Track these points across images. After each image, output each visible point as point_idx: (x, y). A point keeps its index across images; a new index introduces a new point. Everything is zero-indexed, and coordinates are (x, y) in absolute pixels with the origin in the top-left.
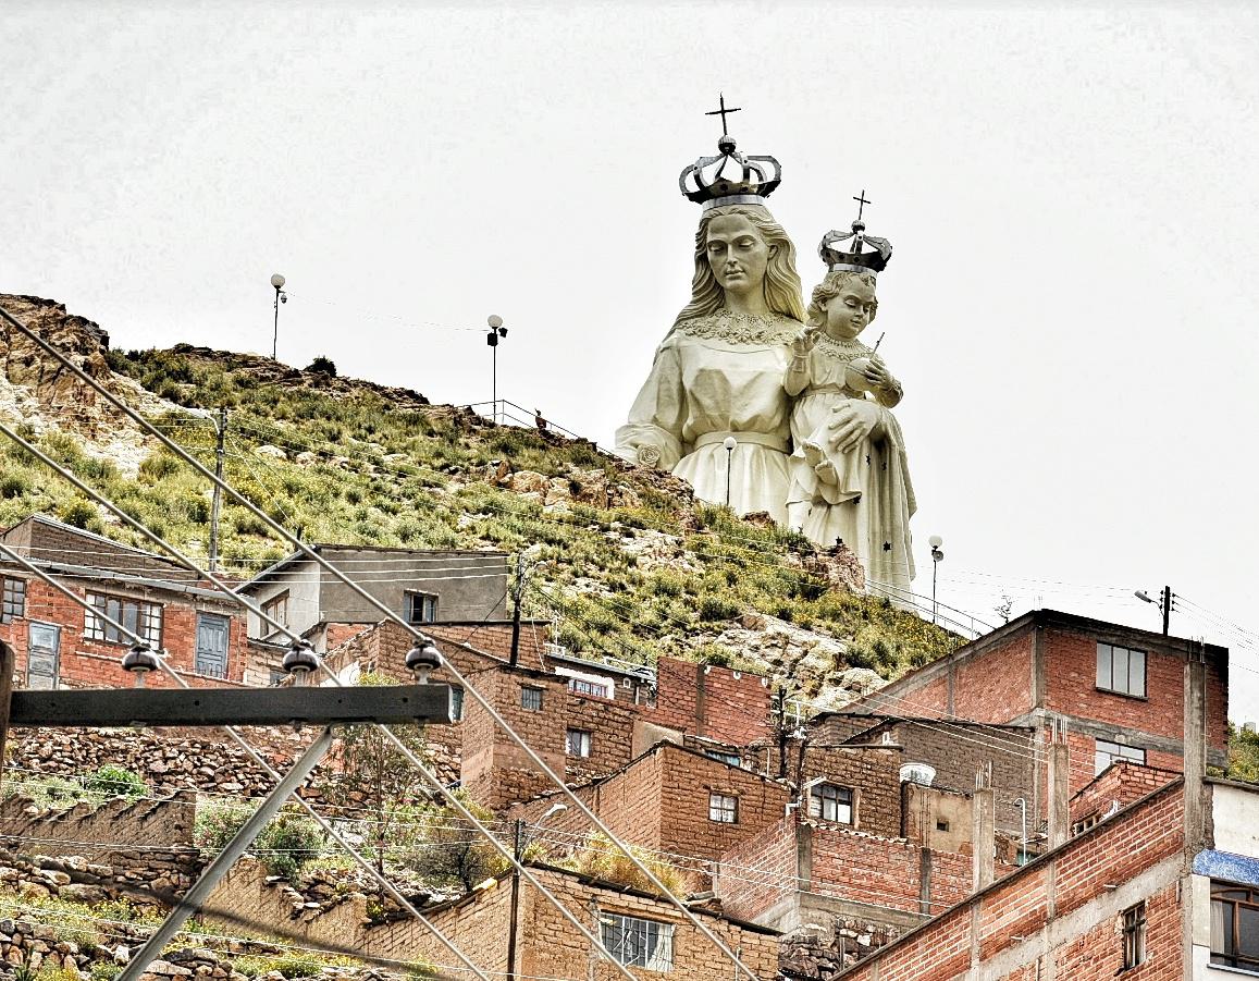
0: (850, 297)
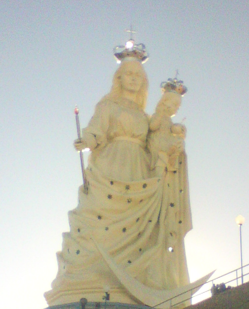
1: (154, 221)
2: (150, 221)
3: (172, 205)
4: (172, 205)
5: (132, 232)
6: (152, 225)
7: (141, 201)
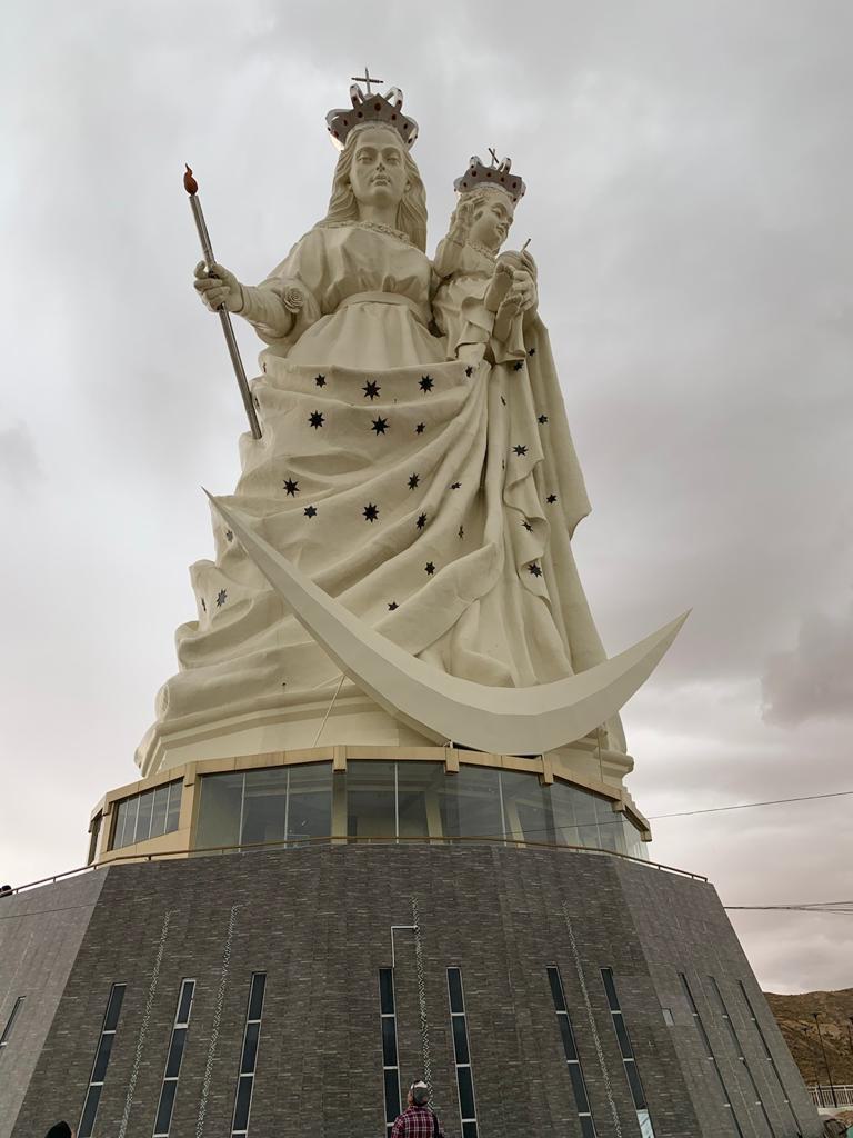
0: (498, 205)
1: (470, 483)
2: (456, 486)
3: (520, 450)
4: (520, 450)
5: (396, 520)
6: (461, 499)
7: (420, 429)
